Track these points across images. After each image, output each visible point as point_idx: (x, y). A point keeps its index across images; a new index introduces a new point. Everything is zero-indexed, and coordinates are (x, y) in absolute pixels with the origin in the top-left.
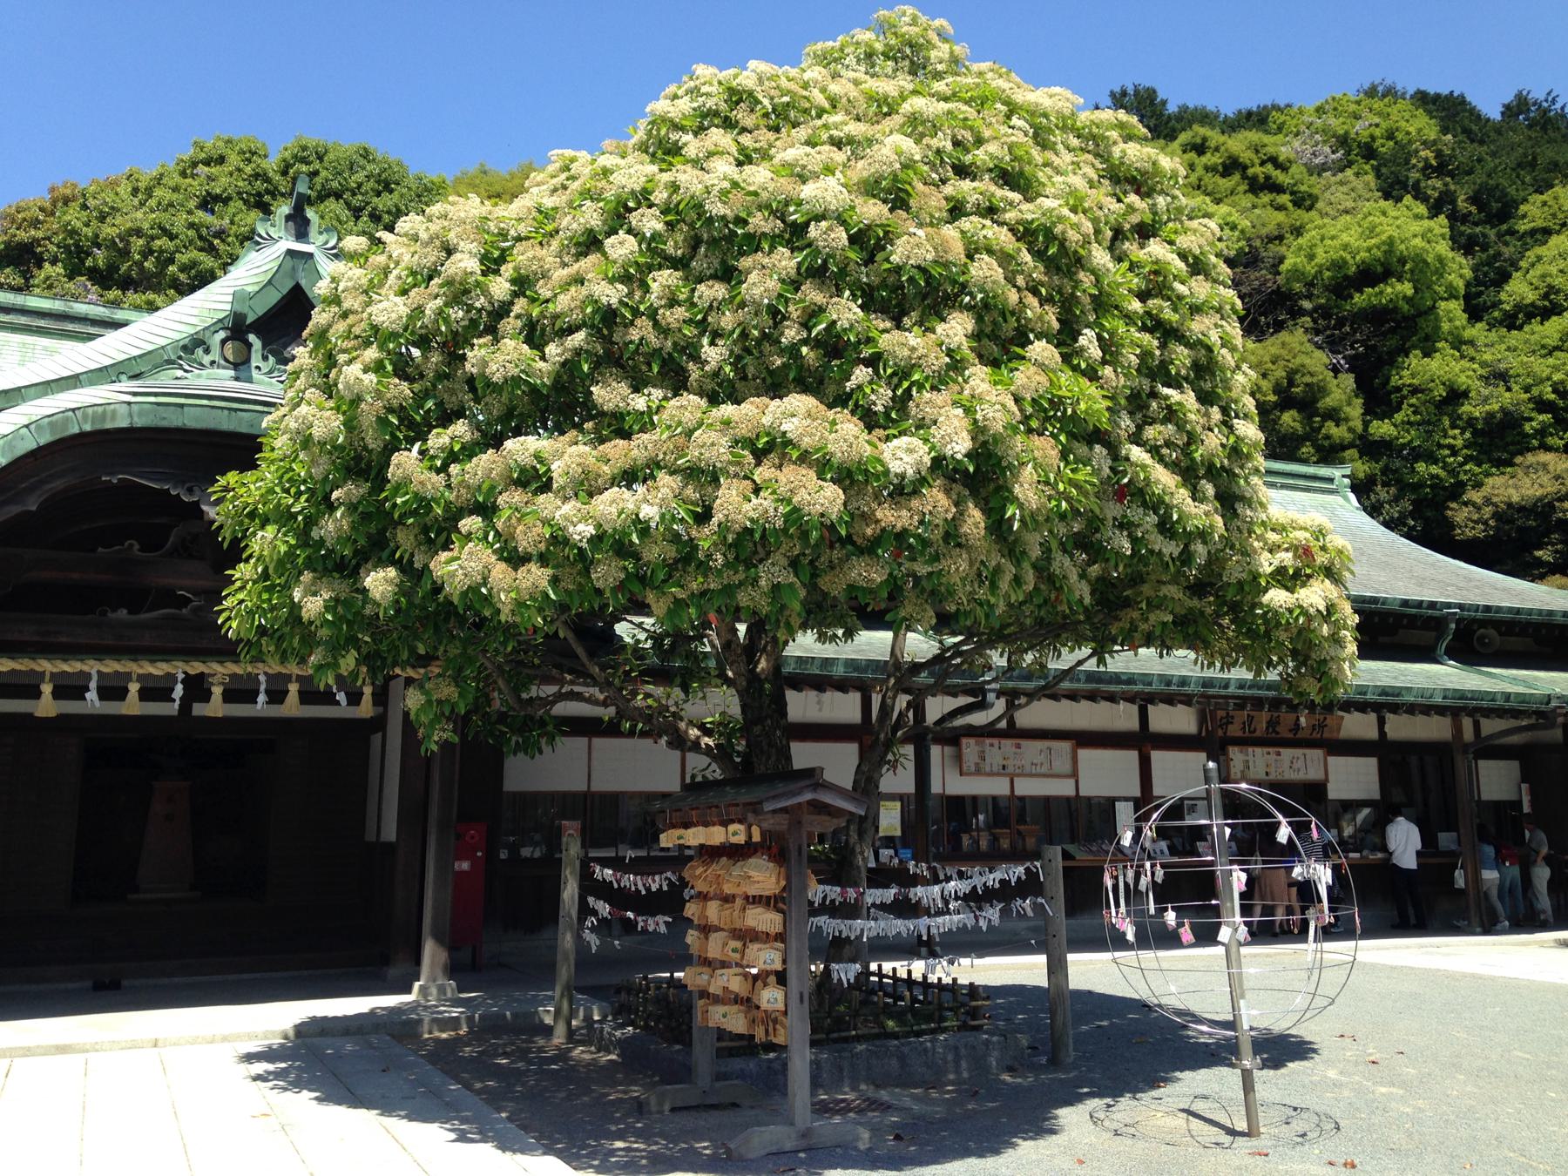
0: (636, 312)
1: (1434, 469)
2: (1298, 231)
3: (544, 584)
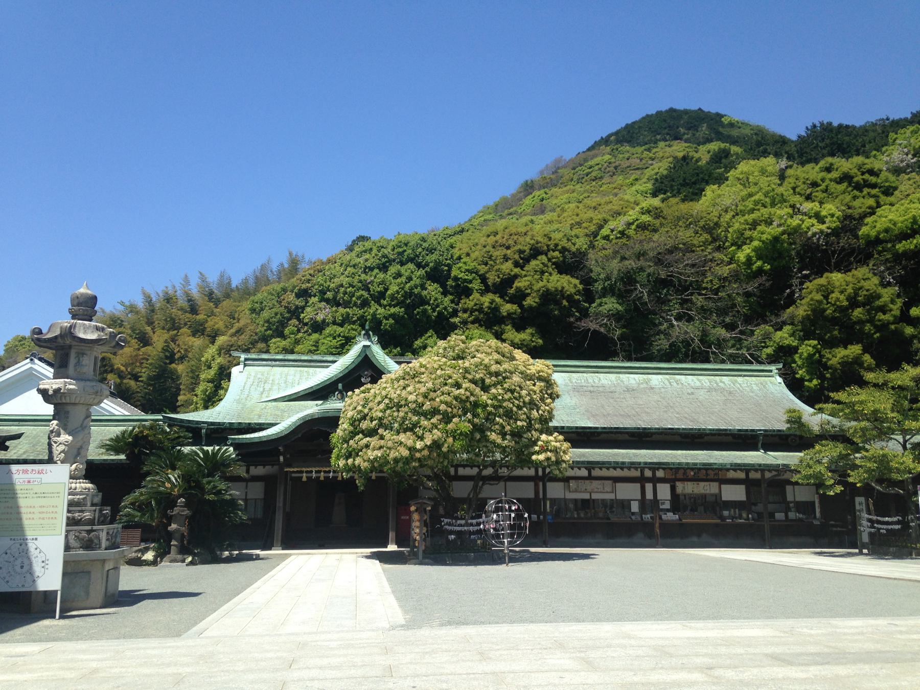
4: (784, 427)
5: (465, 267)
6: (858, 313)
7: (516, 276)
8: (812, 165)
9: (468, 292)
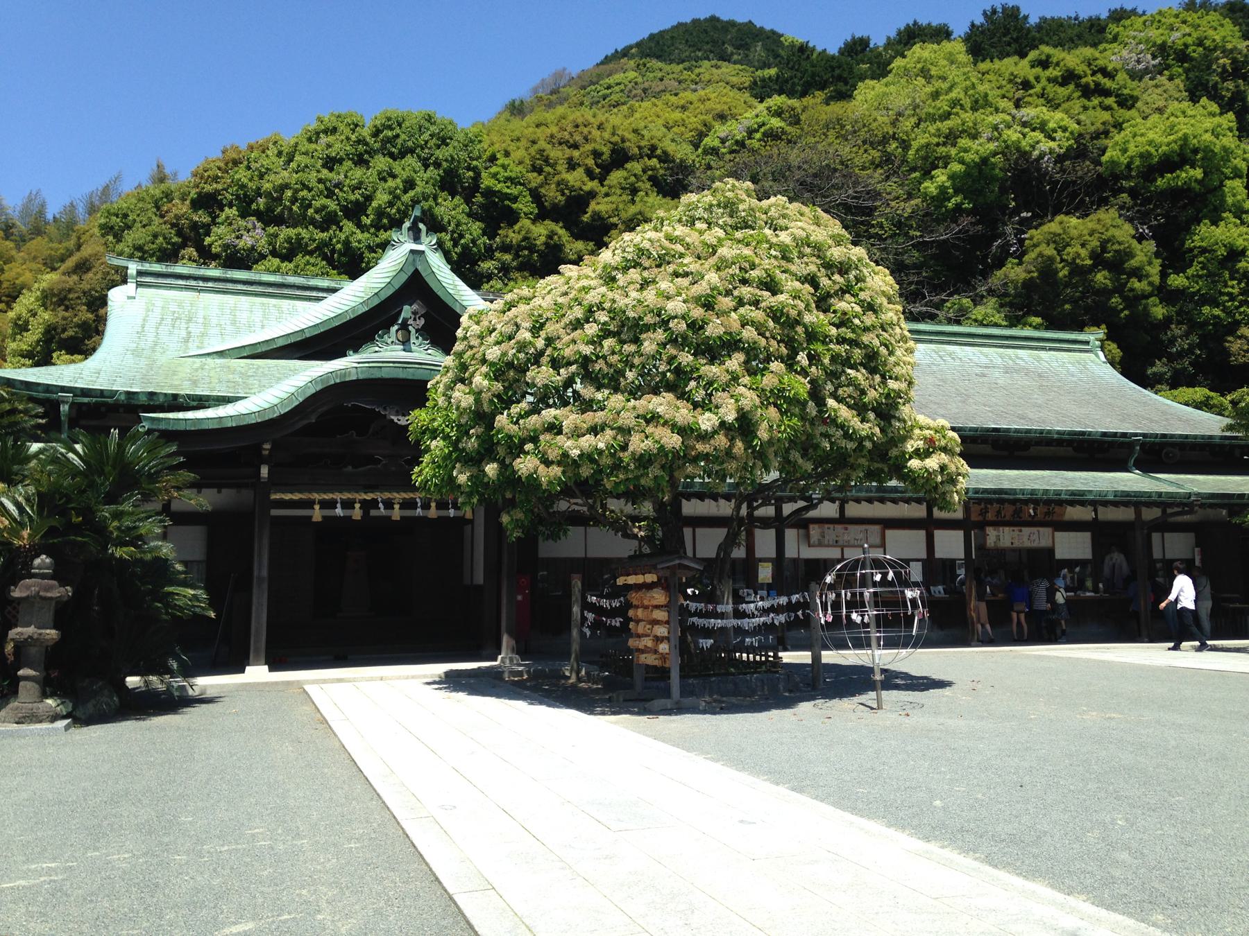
0: (598, 357)
1: (1217, 312)
2: (1119, 126)
3: (560, 474)
5: (503, 174)
7: (592, 195)
9: (512, 218)
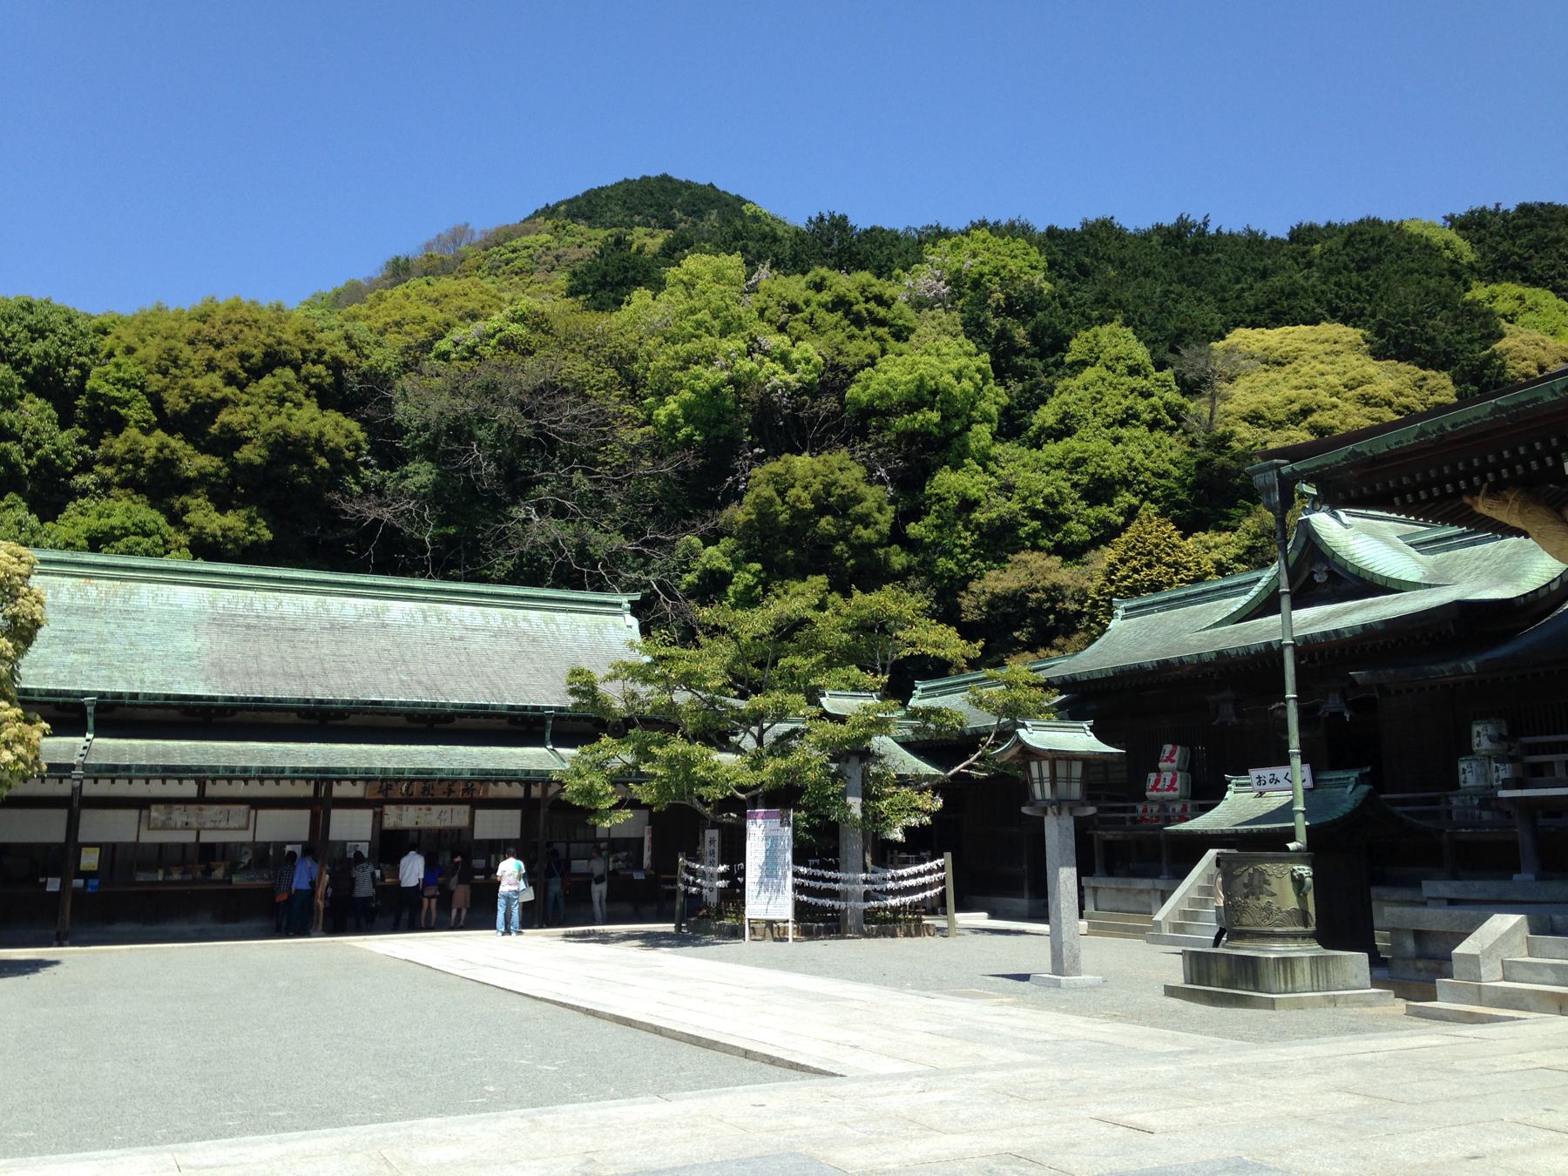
1: (951, 565)
4: (570, 701)
6: (826, 523)
7: (224, 402)
8: (799, 276)
9: (118, 424)
